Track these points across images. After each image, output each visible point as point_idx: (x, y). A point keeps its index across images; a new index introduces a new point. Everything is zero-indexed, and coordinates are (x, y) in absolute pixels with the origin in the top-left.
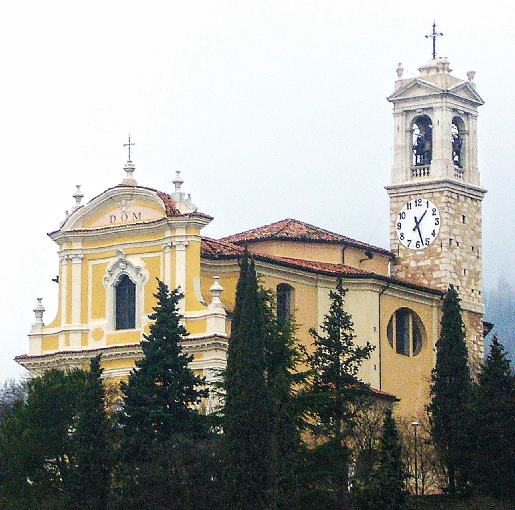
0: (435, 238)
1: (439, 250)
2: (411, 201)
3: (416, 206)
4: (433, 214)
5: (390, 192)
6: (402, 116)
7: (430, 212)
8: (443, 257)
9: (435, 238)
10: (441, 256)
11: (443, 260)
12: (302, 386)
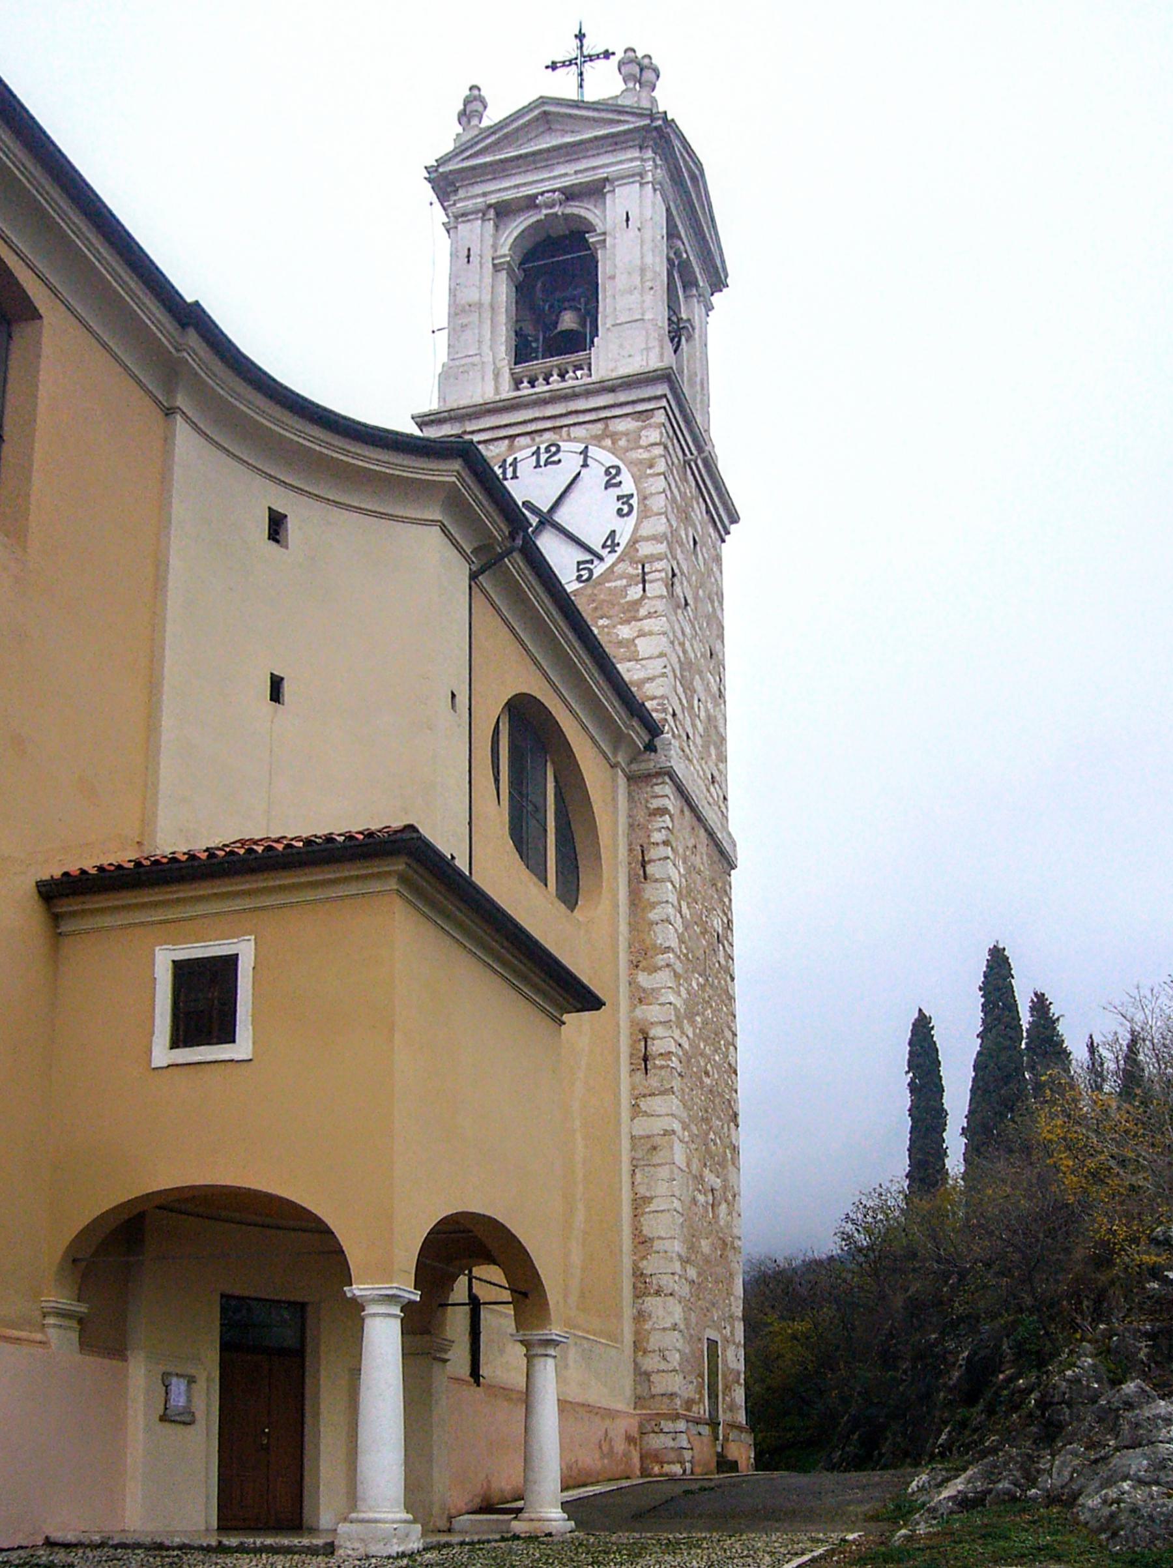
1: (635, 592)
2: (519, 455)
3: (538, 466)
4: (608, 485)
6: (483, 220)
7: (594, 476)
8: (649, 615)
10: (643, 612)
11: (647, 624)
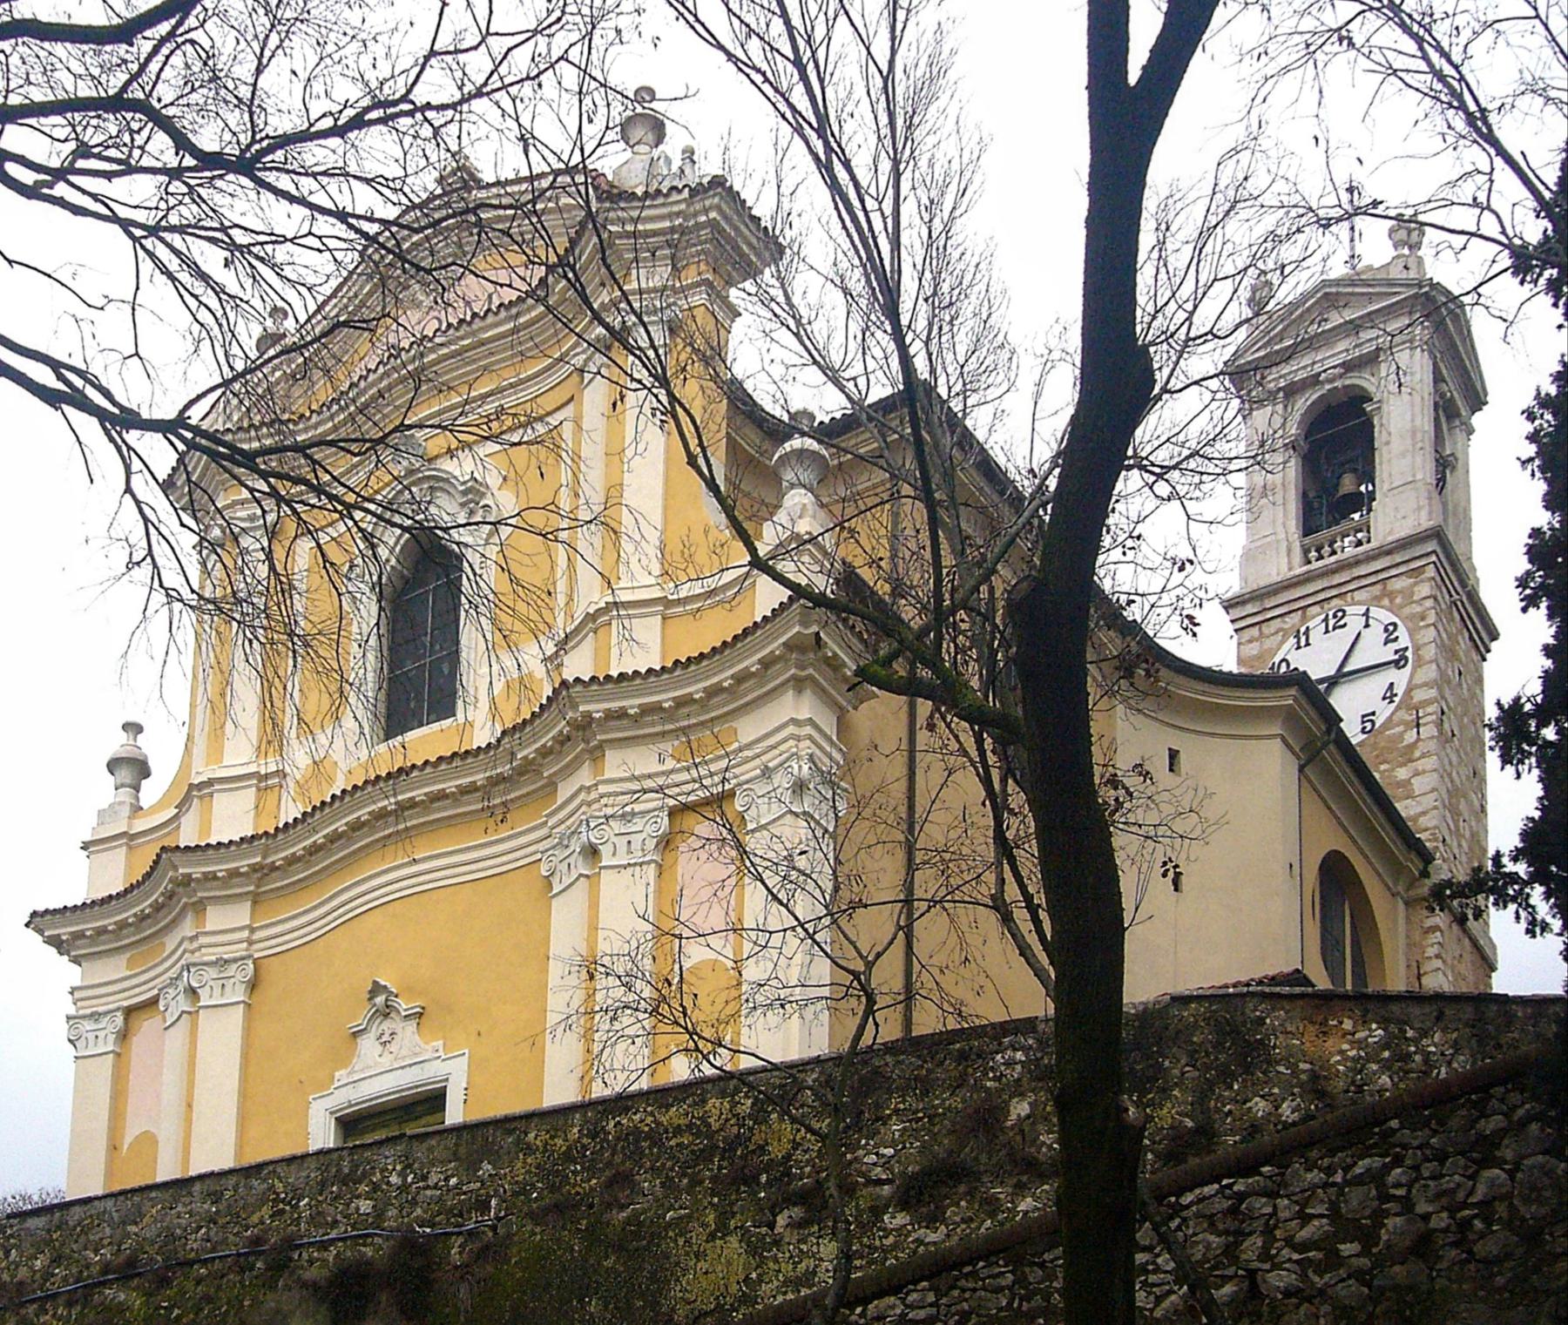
0: (1393, 705)
2: (1311, 624)
3: (1327, 631)
5: (1238, 612)
8: (1423, 756)
9: (1393, 705)
11: (1420, 765)
12: (975, 683)
